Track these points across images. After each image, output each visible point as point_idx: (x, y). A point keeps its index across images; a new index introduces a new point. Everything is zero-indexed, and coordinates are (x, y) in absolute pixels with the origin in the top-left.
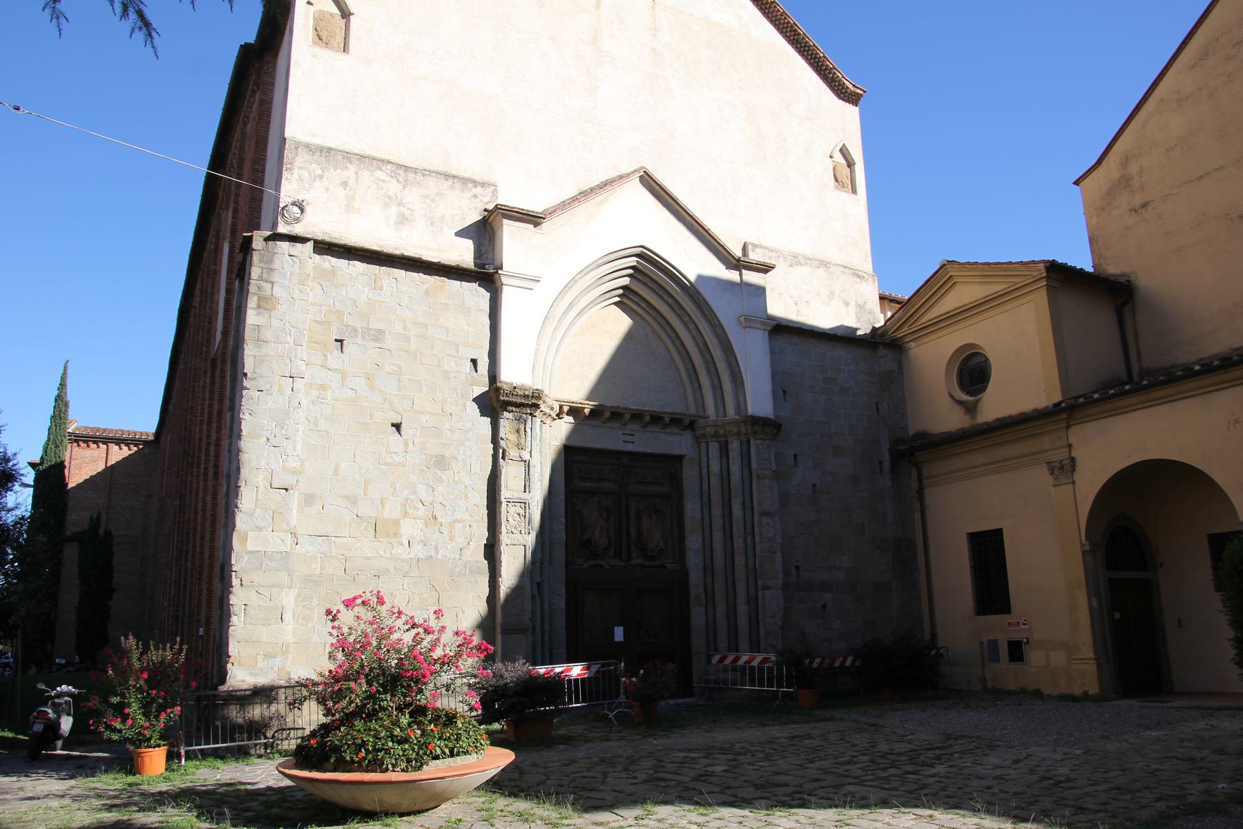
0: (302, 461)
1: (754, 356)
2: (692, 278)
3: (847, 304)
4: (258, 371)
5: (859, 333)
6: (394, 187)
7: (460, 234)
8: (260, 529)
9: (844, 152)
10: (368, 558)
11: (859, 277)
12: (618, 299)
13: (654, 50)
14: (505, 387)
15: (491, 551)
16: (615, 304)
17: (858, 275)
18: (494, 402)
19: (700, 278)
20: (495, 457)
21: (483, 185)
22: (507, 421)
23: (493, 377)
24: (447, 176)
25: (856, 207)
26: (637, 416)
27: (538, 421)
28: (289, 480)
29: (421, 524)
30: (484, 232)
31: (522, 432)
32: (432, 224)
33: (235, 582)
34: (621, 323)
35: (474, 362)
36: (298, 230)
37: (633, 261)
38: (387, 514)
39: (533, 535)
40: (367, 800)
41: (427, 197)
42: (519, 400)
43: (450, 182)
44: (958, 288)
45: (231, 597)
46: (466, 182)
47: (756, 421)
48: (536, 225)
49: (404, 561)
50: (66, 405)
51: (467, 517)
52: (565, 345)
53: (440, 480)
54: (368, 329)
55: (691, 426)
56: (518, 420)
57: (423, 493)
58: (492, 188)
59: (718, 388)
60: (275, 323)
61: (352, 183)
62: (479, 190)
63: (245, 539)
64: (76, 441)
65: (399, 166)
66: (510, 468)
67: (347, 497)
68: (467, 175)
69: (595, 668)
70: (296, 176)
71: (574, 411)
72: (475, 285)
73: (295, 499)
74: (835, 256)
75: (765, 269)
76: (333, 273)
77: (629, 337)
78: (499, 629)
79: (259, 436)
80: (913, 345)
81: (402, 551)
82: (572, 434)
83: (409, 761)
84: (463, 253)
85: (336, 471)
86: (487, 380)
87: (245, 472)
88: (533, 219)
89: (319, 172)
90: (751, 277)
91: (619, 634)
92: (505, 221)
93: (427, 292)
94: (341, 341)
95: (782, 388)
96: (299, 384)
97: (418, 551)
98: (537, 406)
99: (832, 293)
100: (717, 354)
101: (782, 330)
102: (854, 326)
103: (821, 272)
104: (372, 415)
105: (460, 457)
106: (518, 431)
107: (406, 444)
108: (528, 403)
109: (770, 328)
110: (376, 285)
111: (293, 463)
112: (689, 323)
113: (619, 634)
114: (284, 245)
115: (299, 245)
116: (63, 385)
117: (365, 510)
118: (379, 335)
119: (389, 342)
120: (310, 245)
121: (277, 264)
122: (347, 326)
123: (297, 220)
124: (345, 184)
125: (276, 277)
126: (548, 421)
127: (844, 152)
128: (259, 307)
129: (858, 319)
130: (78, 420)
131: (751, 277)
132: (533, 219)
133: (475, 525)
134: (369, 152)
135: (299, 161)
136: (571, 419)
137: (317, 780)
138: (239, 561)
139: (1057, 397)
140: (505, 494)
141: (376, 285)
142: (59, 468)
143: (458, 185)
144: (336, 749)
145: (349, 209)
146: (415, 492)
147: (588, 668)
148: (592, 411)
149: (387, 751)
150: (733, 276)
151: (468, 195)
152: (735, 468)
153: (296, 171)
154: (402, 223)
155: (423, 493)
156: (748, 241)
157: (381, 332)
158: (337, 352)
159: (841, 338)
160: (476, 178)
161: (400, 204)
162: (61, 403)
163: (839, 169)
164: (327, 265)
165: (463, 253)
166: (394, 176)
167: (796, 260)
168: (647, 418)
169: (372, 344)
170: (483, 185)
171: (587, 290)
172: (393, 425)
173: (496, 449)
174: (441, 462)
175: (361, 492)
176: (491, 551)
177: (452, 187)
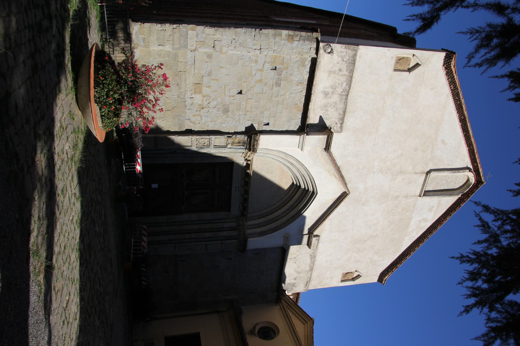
0: (225, 53)
1: (272, 240)
2: (305, 214)
3: (295, 279)
4: (263, 35)
5: (283, 285)
6: (339, 90)
7: (321, 117)
8: (197, 36)
9: (358, 276)
10: (185, 81)
11: (307, 284)
12: (295, 183)
13: (398, 196)
14: (258, 137)
15: (189, 132)
16: (293, 183)
17: (307, 283)
18: (251, 134)
19: (305, 218)
21: (341, 127)
24: (344, 112)
25: (336, 282)
26: (247, 192)
28: (218, 48)
30: (322, 128)
31: (239, 144)
32: (325, 106)
33: (175, 26)
34: (285, 185)
35: (268, 124)
36: (321, 51)
37: (311, 189)
39: (196, 149)
40: (82, 81)
41: (336, 104)
42: (252, 143)
43: (342, 113)
45: (169, 24)
47: (245, 242)
48: (325, 149)
49: (185, 96)
51: (203, 122)
52: (278, 159)
53: (218, 111)
54: (281, 80)
55: (243, 215)
56: (244, 143)
57: (213, 104)
58: (340, 131)
59: (259, 226)
60: (283, 42)
61: (341, 73)
62: (339, 125)
63: (193, 30)
65: (348, 93)
66: (224, 139)
67: (211, 72)
68: (345, 120)
69: (140, 176)
70: (343, 50)
71: (248, 166)
72: (300, 124)
73: (209, 50)
74: (315, 274)
75: (309, 244)
77: (279, 188)
78: (156, 135)
79: (236, 36)
80: (279, 307)
81: (189, 94)
82: (238, 165)
83: (99, 98)
84: (313, 119)
86: (260, 129)
87: (221, 30)
88: (327, 148)
89: (345, 60)
90: (305, 239)
91: (155, 186)
92: (326, 136)
93: (296, 104)
94: (275, 69)
95: (260, 252)
96: (258, 52)
97: (189, 102)
99: (299, 273)
100: (273, 225)
103: (308, 268)
104: (245, 82)
105: (228, 119)
106: (239, 143)
107: (233, 96)
109: (284, 247)
110: (300, 83)
111: (225, 49)
113: (155, 186)
114: (314, 45)
115: (315, 52)
117: (206, 79)
118: (278, 85)
119: (276, 89)
120: (315, 56)
121: (307, 43)
122: (282, 71)
123: (325, 51)
124: (340, 70)
125: (301, 42)
126: (244, 155)
127: (358, 276)
128: (289, 35)
129: (289, 284)
131: (305, 239)
132: (327, 148)
133: (200, 125)
134: (354, 80)
135: (349, 51)
136: (245, 164)
137: (89, 78)
138: (184, 28)
140: (213, 137)
143: (341, 117)
144: (104, 68)
145: (330, 72)
146: (213, 100)
148: (248, 173)
149: (103, 89)
150: (306, 231)
151: (337, 121)
152: (226, 233)
153: (345, 50)
154: (325, 94)
156: (321, 237)
157: (280, 86)
158: (271, 67)
163: (351, 274)
164: (307, 63)
165: (313, 119)
166: (344, 90)
167: (313, 257)
168: (246, 196)
169: (275, 82)
170: (341, 127)
171: (299, 171)
172: (241, 91)
173: (232, 133)
174: (226, 111)
175: (213, 78)
176: (189, 132)
177: (340, 114)
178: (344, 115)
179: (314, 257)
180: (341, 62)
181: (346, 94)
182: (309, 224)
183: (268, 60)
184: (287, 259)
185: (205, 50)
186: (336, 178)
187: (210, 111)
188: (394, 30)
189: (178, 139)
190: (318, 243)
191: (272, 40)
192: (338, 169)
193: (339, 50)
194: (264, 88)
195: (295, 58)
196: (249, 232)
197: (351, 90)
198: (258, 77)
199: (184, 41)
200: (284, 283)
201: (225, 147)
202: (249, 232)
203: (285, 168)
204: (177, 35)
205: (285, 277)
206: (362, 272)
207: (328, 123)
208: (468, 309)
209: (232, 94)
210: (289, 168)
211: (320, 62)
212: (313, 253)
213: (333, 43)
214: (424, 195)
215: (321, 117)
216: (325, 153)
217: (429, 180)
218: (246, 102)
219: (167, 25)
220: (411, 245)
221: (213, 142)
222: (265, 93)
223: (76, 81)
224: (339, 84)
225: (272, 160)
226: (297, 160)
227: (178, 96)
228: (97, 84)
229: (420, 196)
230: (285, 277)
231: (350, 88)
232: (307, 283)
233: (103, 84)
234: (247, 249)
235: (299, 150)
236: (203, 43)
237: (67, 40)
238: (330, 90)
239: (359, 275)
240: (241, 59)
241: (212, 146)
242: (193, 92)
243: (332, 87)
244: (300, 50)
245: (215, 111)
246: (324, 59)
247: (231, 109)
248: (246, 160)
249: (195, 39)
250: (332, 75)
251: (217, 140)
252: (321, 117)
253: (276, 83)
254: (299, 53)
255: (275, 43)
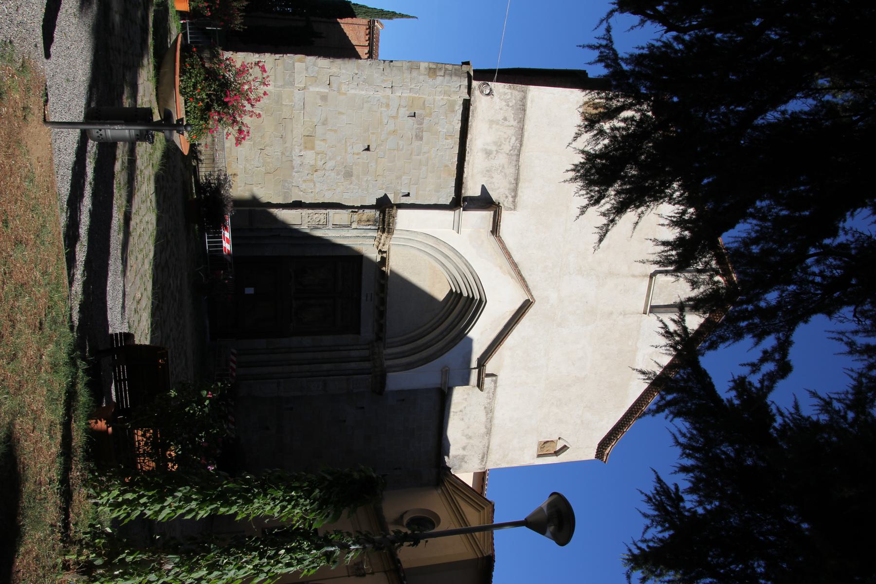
0: (345, 94)
1: (423, 377)
3: (464, 448)
5: (446, 458)
6: (507, 148)
7: (483, 187)
8: (307, 69)
9: (564, 448)
10: (292, 131)
11: (483, 458)
14: (394, 211)
15: (298, 205)
16: (451, 290)
17: (484, 457)
18: (385, 207)
19: (470, 341)
20: (353, 207)
21: (514, 202)
22: (375, 214)
23: (401, 206)
24: (517, 180)
25: (528, 457)
26: (383, 302)
27: (375, 234)
28: (334, 85)
29: (313, 162)
30: (485, 202)
32: (488, 171)
33: (277, 56)
34: (440, 294)
35: (408, 195)
36: (476, 93)
37: (477, 297)
38: (317, 142)
39: (308, 231)
40: (166, 69)
41: (503, 167)
42: (386, 220)
44: (477, 513)
46: (515, 191)
48: (492, 232)
49: (291, 152)
50: (390, 18)
51: (317, 190)
52: (425, 251)
53: (338, 174)
56: (375, 221)
57: (330, 164)
59: (403, 355)
60: (422, 78)
61: (507, 123)
62: (511, 199)
63: (300, 61)
64: (370, 28)
65: (519, 151)
66: (346, 215)
67: (326, 120)
68: (519, 193)
69: (229, 259)
70: (507, 91)
71: (384, 261)
72: (453, 195)
73: (325, 90)
74: (495, 441)
76: (453, 111)
77: (431, 299)
79: (358, 69)
80: (440, 491)
81: (296, 151)
82: (369, 260)
83: (185, 88)
84: (472, 189)
85: (340, 113)
86: (398, 202)
87: (339, 62)
88: (495, 230)
89: (511, 104)
90: (474, 374)
91: (250, 291)
92: (492, 213)
93: (447, 166)
95: (408, 396)
96: (389, 91)
97: (297, 161)
98: (383, 232)
99: (470, 438)
100: (424, 354)
101: (443, 399)
102: (451, 454)
103: (483, 430)
104: (373, 133)
105: (352, 186)
106: (368, 221)
107: (358, 154)
108: (385, 226)
110: (448, 136)
111: (344, 88)
112: (443, 335)
113: (250, 291)
114: (466, 83)
116: (402, 16)
117: (320, 130)
119: (416, 143)
120: (467, 97)
121: (455, 78)
123: (482, 92)
124: (505, 119)
125: (447, 78)
127: (564, 448)
129: (455, 457)
130: (384, 27)
131: (474, 374)
132: (495, 230)
133: (312, 195)
134: (526, 134)
135: (516, 93)
136: (379, 260)
137: (175, 66)
138: (289, 58)
139: (405, 566)
140: (331, 212)
141: (448, 136)
142: (352, 15)
143: (512, 186)
144: (191, 56)
145: (492, 122)
146: (330, 159)
147: (229, 254)
148: (384, 272)
149: (190, 78)
150: (474, 364)
151: (507, 192)
153: (509, 91)
154: (486, 153)
155: (330, 164)
156: (499, 378)
157: (421, 139)
158: (408, 113)
159: (441, 446)
160: (518, 199)
161: (497, 152)
162: (391, 15)
163: (552, 444)
164: (457, 108)
165: (472, 189)
166: (513, 149)
167: (489, 411)
168: (382, 308)
169: (414, 134)
170: (514, 202)
171: (457, 268)
173: (357, 208)
174: (348, 175)
175: (330, 128)
176: (298, 205)
177: (510, 183)
178: (517, 184)
179: (492, 411)
180: (505, 108)
181: (517, 154)
182: (477, 351)
183: (403, 103)
184: (449, 413)
185: (317, 89)
186: (512, 277)
187: (327, 174)
188: (584, 73)
189: (284, 215)
190: (495, 387)
191: (407, 75)
192: (515, 266)
193: (501, 90)
194: (400, 142)
195: (440, 99)
196: (388, 363)
197: (523, 148)
198: (391, 127)
199: (290, 76)
200: (448, 456)
201: (348, 226)
202: (388, 363)
203: (439, 267)
204: (280, 68)
205: (448, 445)
206: (569, 441)
207: (495, 196)
208: (583, 210)
209: (356, 151)
210: (443, 265)
211: (476, 108)
212: (489, 403)
213: (492, 81)
214: (650, 312)
215: (483, 186)
216: (492, 238)
217: (656, 289)
218: (376, 162)
219: (268, 55)
220: (642, 396)
221: (331, 219)
222: (402, 149)
223: (158, 68)
224: (505, 139)
225: (417, 253)
226: (453, 250)
227: (283, 154)
228: (183, 72)
229: (645, 313)
230: (448, 445)
231: (521, 145)
232: (484, 457)
233: (190, 73)
234: (386, 389)
235: (455, 232)
236: (315, 80)
237: (151, 24)
238: (494, 148)
239: (565, 446)
240: (367, 102)
241: (330, 226)
242: (302, 147)
243: (495, 143)
244: (447, 88)
245: (333, 174)
246: (482, 105)
247: (355, 172)
248: (380, 251)
249: (305, 74)
250: (494, 126)
251: (337, 216)
252: (483, 186)
253: (416, 136)
254: (445, 93)
255: (411, 79)
